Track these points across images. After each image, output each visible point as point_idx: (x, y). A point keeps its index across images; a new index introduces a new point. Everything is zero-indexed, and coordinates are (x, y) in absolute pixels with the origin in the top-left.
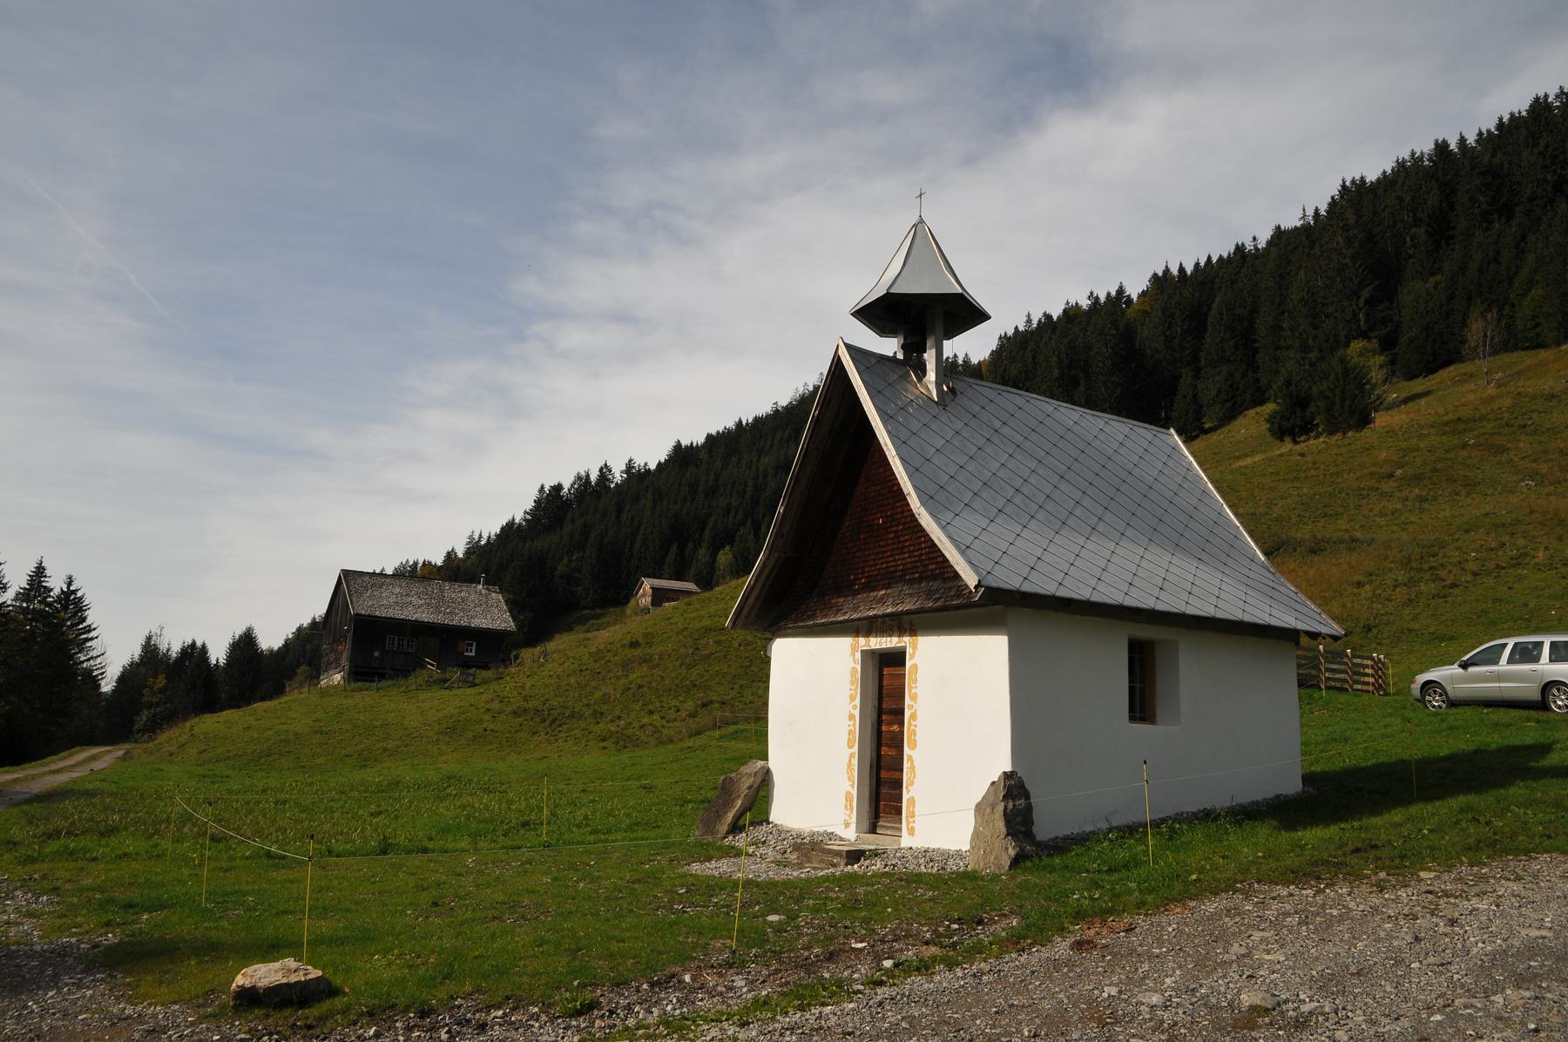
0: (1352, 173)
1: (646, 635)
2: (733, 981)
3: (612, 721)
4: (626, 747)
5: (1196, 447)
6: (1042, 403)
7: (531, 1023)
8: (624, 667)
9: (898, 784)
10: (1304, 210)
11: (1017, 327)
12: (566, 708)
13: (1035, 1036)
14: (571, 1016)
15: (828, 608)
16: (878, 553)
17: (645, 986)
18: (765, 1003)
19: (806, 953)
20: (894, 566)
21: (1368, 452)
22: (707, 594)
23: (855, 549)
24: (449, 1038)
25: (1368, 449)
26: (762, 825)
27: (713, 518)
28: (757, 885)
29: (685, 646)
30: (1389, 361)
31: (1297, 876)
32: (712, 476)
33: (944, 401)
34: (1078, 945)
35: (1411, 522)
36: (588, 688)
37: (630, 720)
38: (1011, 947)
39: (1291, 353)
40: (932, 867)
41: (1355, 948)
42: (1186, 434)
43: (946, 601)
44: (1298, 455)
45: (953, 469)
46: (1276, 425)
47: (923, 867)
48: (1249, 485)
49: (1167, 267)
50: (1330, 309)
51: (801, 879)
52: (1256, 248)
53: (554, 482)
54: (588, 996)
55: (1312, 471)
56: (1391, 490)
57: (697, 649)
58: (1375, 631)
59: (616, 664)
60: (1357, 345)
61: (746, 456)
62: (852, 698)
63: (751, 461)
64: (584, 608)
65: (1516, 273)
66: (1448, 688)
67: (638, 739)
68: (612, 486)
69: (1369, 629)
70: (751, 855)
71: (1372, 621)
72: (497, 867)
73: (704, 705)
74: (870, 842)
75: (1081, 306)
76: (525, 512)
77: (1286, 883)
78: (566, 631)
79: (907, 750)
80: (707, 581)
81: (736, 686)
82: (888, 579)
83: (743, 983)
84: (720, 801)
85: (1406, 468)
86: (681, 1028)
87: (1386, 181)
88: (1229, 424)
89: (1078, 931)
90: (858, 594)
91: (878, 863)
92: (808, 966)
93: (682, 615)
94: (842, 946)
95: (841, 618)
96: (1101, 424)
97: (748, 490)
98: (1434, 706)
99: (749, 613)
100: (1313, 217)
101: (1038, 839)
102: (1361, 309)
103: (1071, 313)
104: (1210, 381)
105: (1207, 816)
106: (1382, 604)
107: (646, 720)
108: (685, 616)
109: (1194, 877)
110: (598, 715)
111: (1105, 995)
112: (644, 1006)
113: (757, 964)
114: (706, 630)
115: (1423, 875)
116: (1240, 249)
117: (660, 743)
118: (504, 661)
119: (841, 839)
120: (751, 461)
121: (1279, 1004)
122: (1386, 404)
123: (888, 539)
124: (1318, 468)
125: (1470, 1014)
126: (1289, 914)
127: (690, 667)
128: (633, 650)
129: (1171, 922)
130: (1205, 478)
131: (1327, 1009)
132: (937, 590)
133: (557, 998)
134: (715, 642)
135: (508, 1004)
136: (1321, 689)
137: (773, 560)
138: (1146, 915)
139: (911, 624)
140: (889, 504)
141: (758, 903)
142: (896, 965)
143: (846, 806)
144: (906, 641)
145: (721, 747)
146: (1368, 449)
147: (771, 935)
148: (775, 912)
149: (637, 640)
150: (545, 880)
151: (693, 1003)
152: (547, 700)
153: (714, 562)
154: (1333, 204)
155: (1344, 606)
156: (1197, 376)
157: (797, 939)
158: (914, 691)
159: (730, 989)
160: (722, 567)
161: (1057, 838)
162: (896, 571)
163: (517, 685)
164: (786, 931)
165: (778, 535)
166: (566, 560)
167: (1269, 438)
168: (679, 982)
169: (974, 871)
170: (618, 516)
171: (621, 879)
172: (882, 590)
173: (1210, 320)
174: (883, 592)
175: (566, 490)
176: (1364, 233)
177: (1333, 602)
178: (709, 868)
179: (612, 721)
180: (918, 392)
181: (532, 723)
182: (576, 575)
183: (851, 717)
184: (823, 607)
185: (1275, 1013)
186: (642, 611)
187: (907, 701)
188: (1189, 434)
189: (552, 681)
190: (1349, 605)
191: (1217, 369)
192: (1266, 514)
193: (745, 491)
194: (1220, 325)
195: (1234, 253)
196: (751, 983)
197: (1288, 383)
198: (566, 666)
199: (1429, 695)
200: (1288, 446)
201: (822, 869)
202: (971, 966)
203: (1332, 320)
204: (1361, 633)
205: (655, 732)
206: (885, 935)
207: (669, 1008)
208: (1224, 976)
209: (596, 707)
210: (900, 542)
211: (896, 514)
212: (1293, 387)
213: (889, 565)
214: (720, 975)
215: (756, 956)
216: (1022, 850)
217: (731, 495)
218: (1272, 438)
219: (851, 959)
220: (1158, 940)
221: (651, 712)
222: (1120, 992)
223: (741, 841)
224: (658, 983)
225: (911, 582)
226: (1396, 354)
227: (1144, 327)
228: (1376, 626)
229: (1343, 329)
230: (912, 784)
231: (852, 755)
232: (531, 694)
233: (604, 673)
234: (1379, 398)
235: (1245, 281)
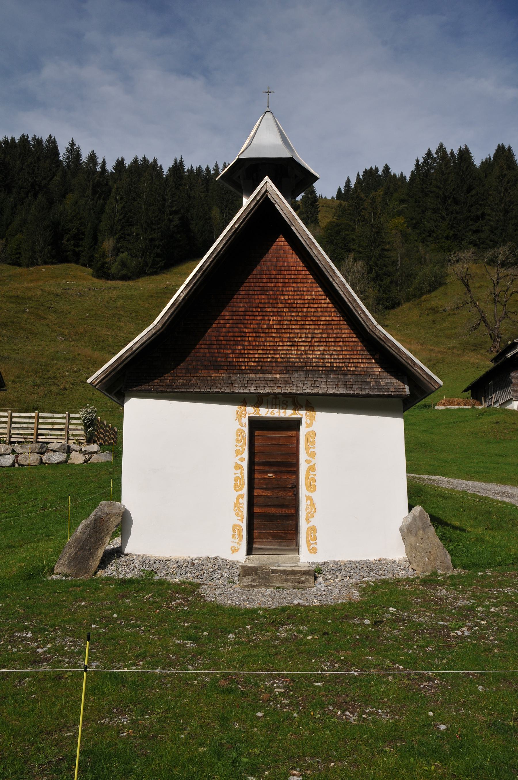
65: (10, 223)
144: (302, 414)
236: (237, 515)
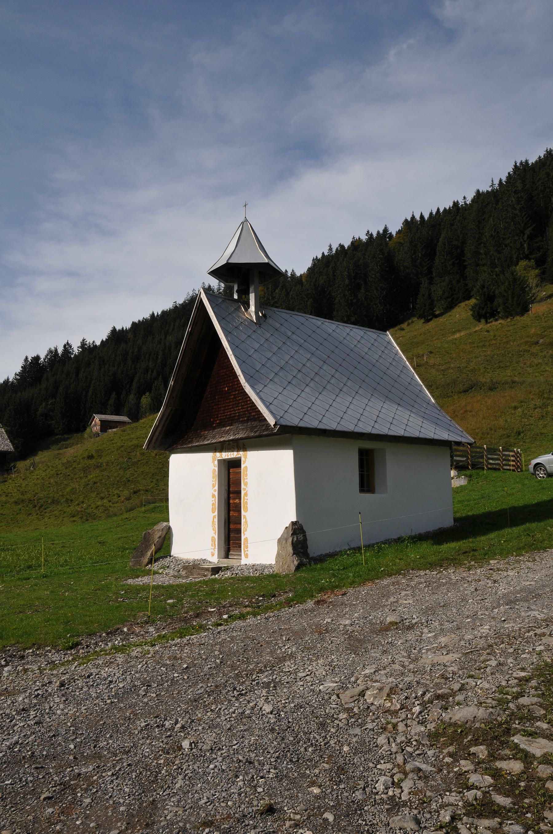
0: (520, 158)
1: (97, 451)
2: (148, 629)
3: (78, 504)
4: (87, 520)
5: (430, 326)
6: (314, 320)
7: (47, 654)
8: (84, 471)
9: (239, 531)
10: (492, 181)
11: (323, 253)
12: (49, 498)
13: (288, 640)
14: (67, 649)
15: (200, 437)
16: (225, 407)
17: (104, 635)
18: (164, 637)
19: (186, 615)
20: (234, 413)
21: (525, 329)
22: (134, 425)
23: (213, 404)
24: (6, 663)
25: (525, 327)
26: (167, 558)
27: (138, 375)
28: (163, 587)
29: (122, 457)
30: (541, 273)
31: (431, 566)
32: (136, 349)
33: (259, 322)
34: (318, 603)
35: (546, 371)
36: (62, 485)
37: (89, 503)
38: (286, 606)
39: (485, 268)
40: (256, 573)
41: (447, 596)
42: (425, 318)
43: (260, 432)
44: (485, 332)
45: (264, 361)
46: (476, 313)
47: (251, 574)
48: (457, 350)
49: (413, 215)
50: (508, 242)
51: (187, 583)
52: (466, 204)
53: (34, 355)
54: (76, 640)
55: (493, 341)
56: (536, 351)
57: (130, 458)
58: (522, 435)
59: (79, 470)
60: (523, 263)
61: (157, 336)
62: (214, 486)
63: (161, 339)
64: (57, 434)
66: (547, 467)
67: (95, 515)
68: (72, 356)
69: (519, 433)
70: (161, 574)
71: (521, 430)
72: (17, 589)
73: (135, 493)
74: (225, 563)
75: (362, 240)
76: (16, 374)
77: (425, 569)
78: (46, 449)
79: (243, 513)
80: (135, 416)
81: (154, 480)
82: (230, 421)
83: (153, 629)
84: (143, 546)
85: (545, 338)
86: (122, 649)
87: (541, 163)
88: (450, 311)
89: (319, 596)
90: (215, 429)
91: (229, 573)
92: (185, 620)
93: (120, 438)
94: (203, 611)
95: (206, 443)
96: (348, 330)
97: (159, 357)
98: (540, 477)
99: (156, 440)
100: (499, 184)
101: (311, 555)
102: (525, 241)
103: (356, 244)
104: (439, 285)
105: (399, 540)
106: (527, 419)
107: (99, 503)
108: (122, 438)
109: (382, 569)
110: (69, 502)
111: (325, 622)
112: (104, 642)
113: (161, 621)
114: (135, 446)
115: (491, 562)
116: (456, 204)
117: (109, 516)
118: (7, 470)
119: (210, 562)
120: (161, 339)
121: (402, 620)
122: (538, 298)
123: (230, 399)
124: (497, 339)
125: (482, 617)
126: (422, 583)
127: (125, 469)
128: (90, 461)
129: (364, 590)
130: (405, 359)
131: (423, 621)
132: (256, 426)
133: (60, 642)
134: (141, 454)
135: (34, 647)
136: (483, 469)
137: (168, 411)
138: (354, 587)
139: (244, 445)
140: (230, 380)
141: (163, 595)
142: (229, 617)
143: (212, 544)
144: (241, 454)
145: (145, 517)
146: (525, 327)
147: (168, 609)
148: (171, 598)
149: (92, 454)
150: (46, 593)
151: (128, 639)
152: (37, 494)
153: (139, 403)
154: (509, 176)
155: (506, 421)
156: (431, 283)
157: (182, 609)
158: (246, 480)
159: (147, 632)
160: (144, 406)
161: (321, 555)
162: (235, 416)
163: (17, 485)
164: (176, 606)
165: (171, 397)
166: (44, 404)
167: (472, 320)
168: (121, 631)
169: (277, 574)
170: (77, 375)
171: (89, 589)
172: (227, 427)
173: (438, 248)
174: (228, 428)
175: (42, 360)
176: (527, 195)
177: (500, 419)
178: (137, 581)
179: (78, 504)
180: (245, 317)
181: (27, 508)
182: (51, 413)
183: (213, 496)
184: (196, 436)
185: (400, 624)
186: (94, 435)
187: (243, 486)
188: (426, 318)
189: (39, 481)
190: (509, 420)
191: (443, 278)
192: (466, 367)
193: (157, 358)
194: (444, 252)
195: (453, 207)
196: (157, 630)
197: (483, 287)
198: (47, 472)
199: (538, 471)
200: (482, 326)
201: (198, 578)
202: (265, 614)
203: (509, 248)
204: (514, 436)
205: (105, 510)
206: (226, 604)
207: (116, 642)
208: (382, 611)
209: (68, 497)
210: (236, 400)
211: (235, 385)
212: (485, 289)
213: (231, 413)
214: (142, 627)
215: (160, 618)
216: (301, 561)
217: (149, 361)
218: (474, 320)
219: (208, 616)
220: (356, 598)
221: (102, 498)
222: (332, 620)
223: (155, 567)
224: (111, 633)
225: (243, 422)
226: (546, 268)
227: (400, 253)
228: (523, 432)
229: (515, 253)
230: (246, 530)
231: (214, 517)
232: (26, 490)
233: (72, 475)
234: (533, 296)
235: (458, 224)
236: (213, 530)
